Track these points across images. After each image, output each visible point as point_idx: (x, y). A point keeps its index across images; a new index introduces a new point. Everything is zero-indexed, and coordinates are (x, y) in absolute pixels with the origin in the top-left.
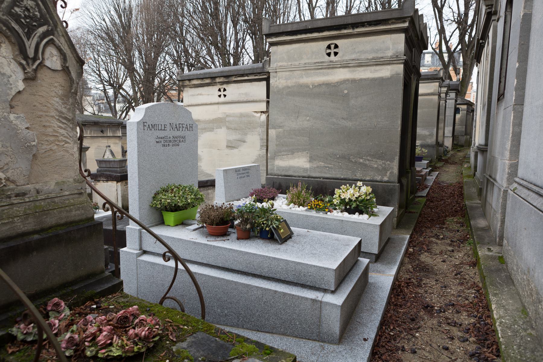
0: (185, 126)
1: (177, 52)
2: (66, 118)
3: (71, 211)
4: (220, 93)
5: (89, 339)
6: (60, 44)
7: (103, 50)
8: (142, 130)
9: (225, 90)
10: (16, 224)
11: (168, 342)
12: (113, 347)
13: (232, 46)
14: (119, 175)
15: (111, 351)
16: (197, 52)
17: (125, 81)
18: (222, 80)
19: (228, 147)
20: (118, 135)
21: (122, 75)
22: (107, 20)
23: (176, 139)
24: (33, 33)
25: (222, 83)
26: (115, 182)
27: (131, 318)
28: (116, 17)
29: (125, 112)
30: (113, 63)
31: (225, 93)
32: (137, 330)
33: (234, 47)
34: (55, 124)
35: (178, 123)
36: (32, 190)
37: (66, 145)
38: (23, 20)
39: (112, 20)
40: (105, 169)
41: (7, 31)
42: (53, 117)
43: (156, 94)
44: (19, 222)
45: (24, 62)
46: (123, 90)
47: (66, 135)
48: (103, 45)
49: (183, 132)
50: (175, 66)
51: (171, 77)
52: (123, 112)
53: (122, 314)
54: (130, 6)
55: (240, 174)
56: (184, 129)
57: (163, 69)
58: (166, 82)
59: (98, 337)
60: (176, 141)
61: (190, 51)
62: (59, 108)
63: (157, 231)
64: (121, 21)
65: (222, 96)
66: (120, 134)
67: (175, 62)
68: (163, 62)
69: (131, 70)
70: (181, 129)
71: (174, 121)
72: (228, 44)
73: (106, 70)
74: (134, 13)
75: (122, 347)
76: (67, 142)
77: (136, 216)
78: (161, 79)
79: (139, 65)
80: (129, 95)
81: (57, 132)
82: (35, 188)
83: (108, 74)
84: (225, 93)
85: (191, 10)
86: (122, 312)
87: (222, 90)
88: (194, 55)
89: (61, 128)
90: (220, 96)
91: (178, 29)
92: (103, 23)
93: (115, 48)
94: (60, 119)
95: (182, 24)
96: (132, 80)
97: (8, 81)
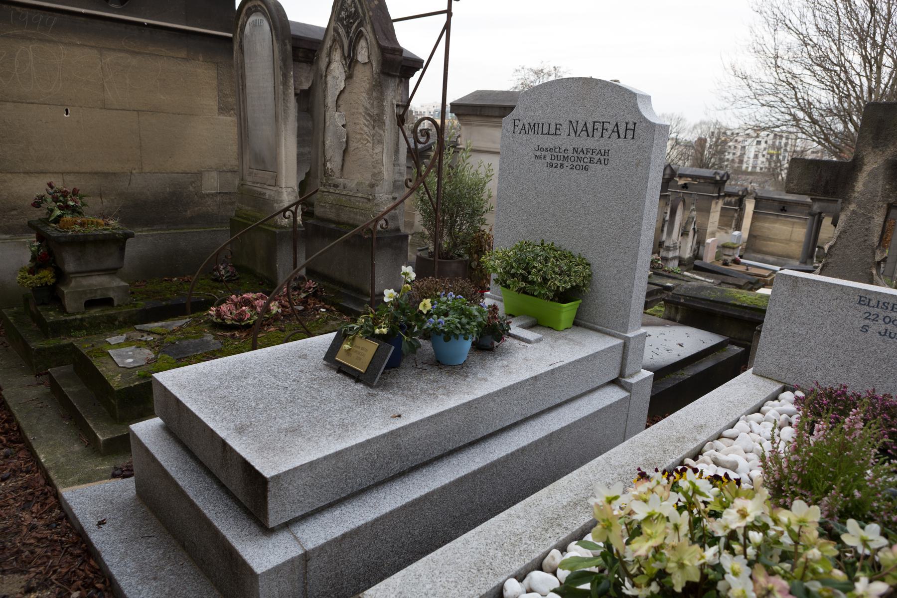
0: (610, 127)
3: (356, 214)
8: (511, 134)
49: (602, 141)
70: (598, 134)
71: (581, 117)
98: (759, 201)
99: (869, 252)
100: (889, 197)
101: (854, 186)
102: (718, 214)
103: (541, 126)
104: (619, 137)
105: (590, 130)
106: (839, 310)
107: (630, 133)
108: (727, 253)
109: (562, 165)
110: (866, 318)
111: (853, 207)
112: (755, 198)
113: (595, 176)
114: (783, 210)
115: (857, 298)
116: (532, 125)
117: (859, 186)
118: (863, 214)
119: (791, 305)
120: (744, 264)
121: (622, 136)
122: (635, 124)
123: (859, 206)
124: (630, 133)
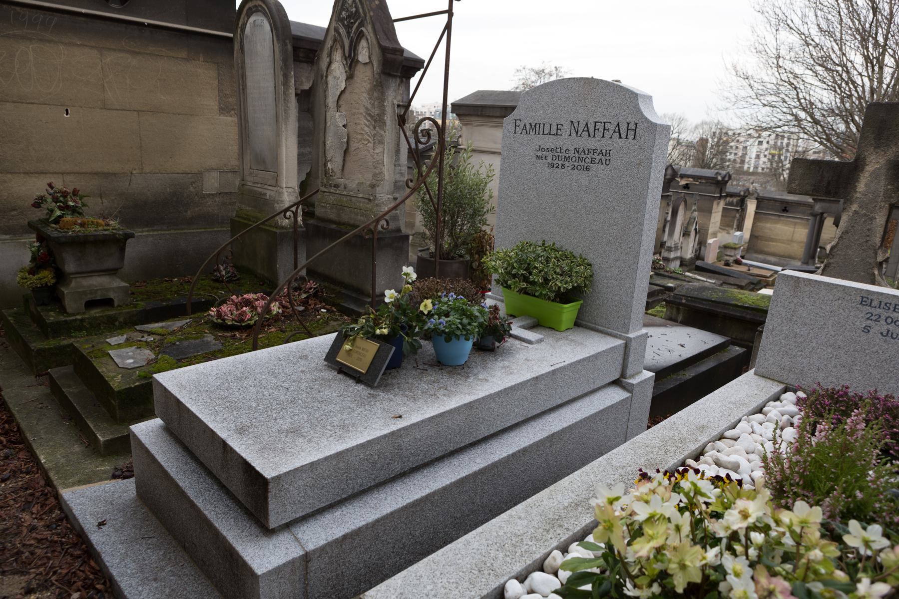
0: (611, 127)
3: (357, 214)
8: (512, 134)
49: (603, 141)
70: (599, 134)
71: (582, 117)
98: (761, 201)
99: (871, 252)
100: (891, 197)
101: (856, 186)
102: (720, 214)
103: (542, 126)
104: (620, 137)
105: (591, 130)
106: (841, 311)
107: (631, 133)
108: (728, 253)
109: (563, 165)
110: (868, 319)
111: (854, 207)
112: (757, 199)
113: (596, 176)
114: (785, 210)
115: (859, 299)
116: (533, 125)
117: (861, 187)
118: (865, 215)
119: (792, 305)
120: (746, 264)
121: (624, 136)
122: (636, 124)
123: (861, 207)
124: (631, 133)
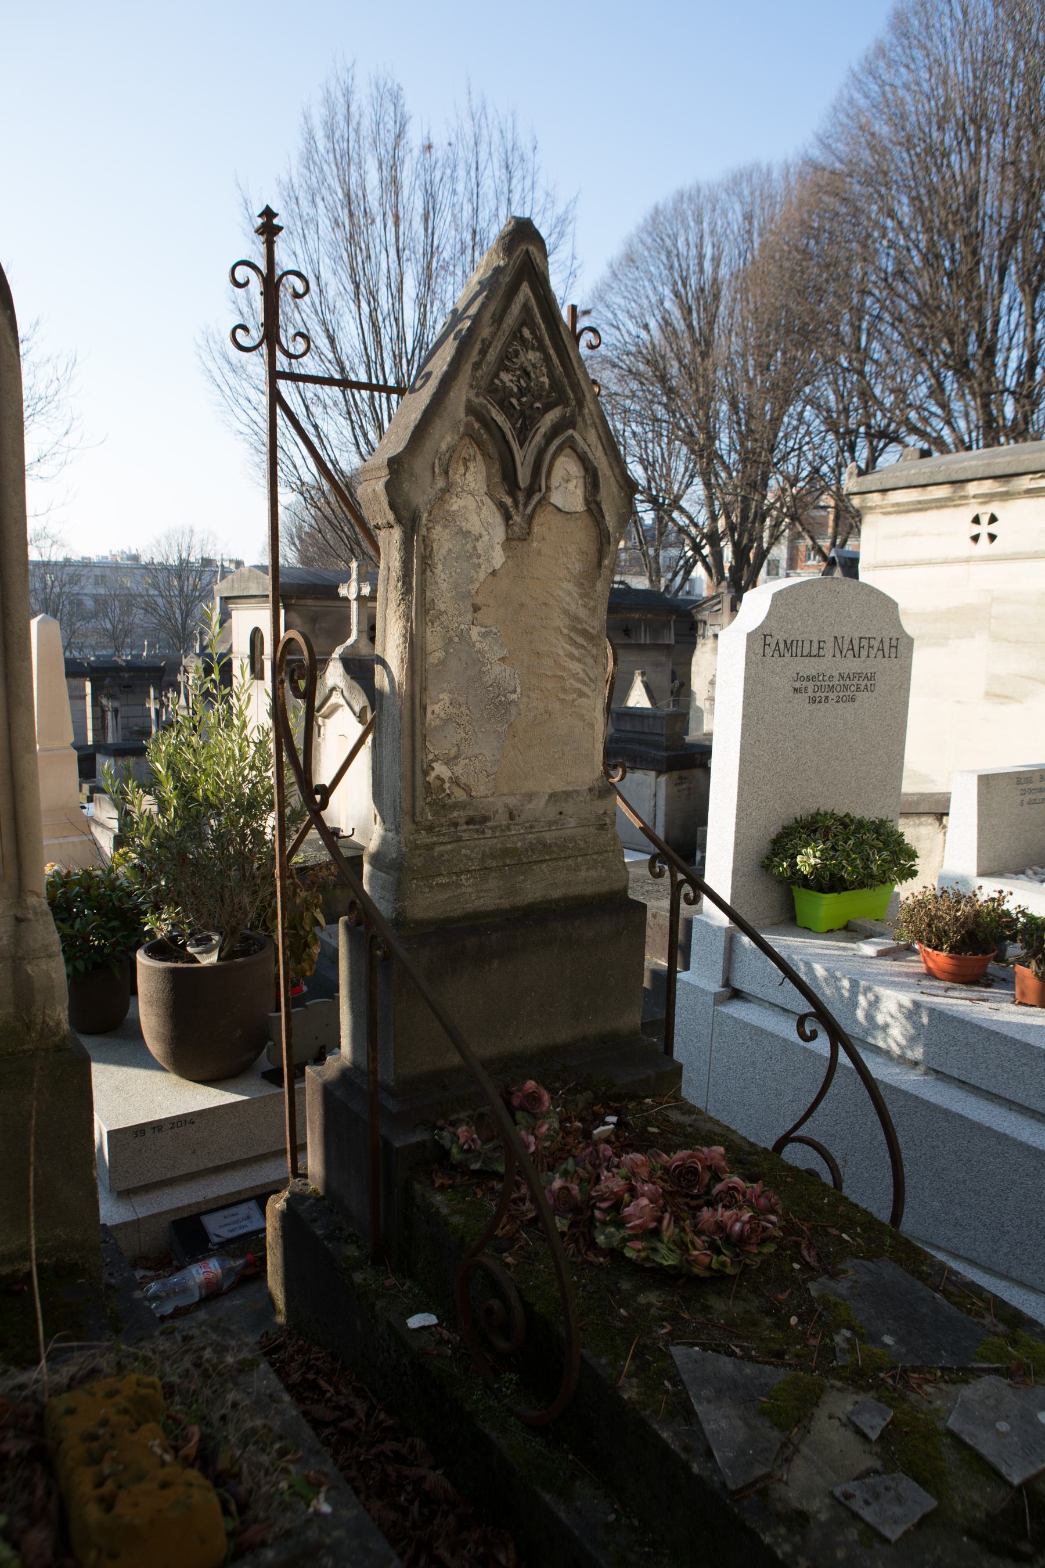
0: (876, 644)
1: (840, 396)
2: (585, 633)
3: (577, 869)
4: (976, 529)
5: (604, 1205)
6: (586, 448)
7: (638, 408)
8: (759, 657)
9: (993, 519)
10: (464, 889)
11: (796, 1266)
12: (662, 1242)
13: (1013, 365)
14: (664, 754)
15: (655, 1250)
16: (900, 393)
17: (688, 486)
18: (987, 486)
19: (989, 695)
20: (667, 642)
21: (682, 470)
22: (653, 324)
23: (848, 682)
24: (532, 428)
25: (989, 498)
26: (653, 774)
27: (707, 1177)
28: (676, 314)
29: (682, 573)
30: (660, 440)
31: (993, 529)
32: (723, 1214)
33: (1018, 368)
34: (562, 647)
35: (856, 635)
36: (500, 811)
37: (580, 701)
38: (514, 401)
39: (666, 323)
40: (630, 735)
41: (482, 431)
42: (557, 629)
43: (768, 521)
44: (469, 886)
45: (508, 501)
46: (682, 510)
47: (582, 675)
48: (640, 394)
49: (869, 662)
50: (830, 437)
51: (816, 470)
52: (675, 574)
53: (682, 1159)
54: (715, 280)
55: (1031, 791)
56: (873, 653)
57: (793, 450)
58: (801, 484)
59: (628, 1205)
60: (849, 688)
61: (877, 391)
62: (573, 607)
63: (783, 943)
64: (690, 327)
65: (984, 539)
66: (670, 639)
67: (832, 426)
68: (796, 428)
69: (705, 457)
70: (864, 653)
71: (848, 631)
72: (999, 359)
73: (641, 461)
74: (726, 294)
75: (682, 1246)
76: (582, 694)
77: (725, 894)
78: (786, 478)
79: (727, 440)
80: (696, 525)
81: (564, 669)
82: (506, 806)
83: (646, 469)
84: (993, 529)
85: (890, 269)
86: (682, 1154)
87: (985, 519)
88: (889, 400)
89: (572, 657)
90: (975, 538)
91: (845, 329)
92: (644, 334)
93: (669, 398)
94: (572, 635)
95: (859, 312)
96: (708, 485)
97: (475, 548)
